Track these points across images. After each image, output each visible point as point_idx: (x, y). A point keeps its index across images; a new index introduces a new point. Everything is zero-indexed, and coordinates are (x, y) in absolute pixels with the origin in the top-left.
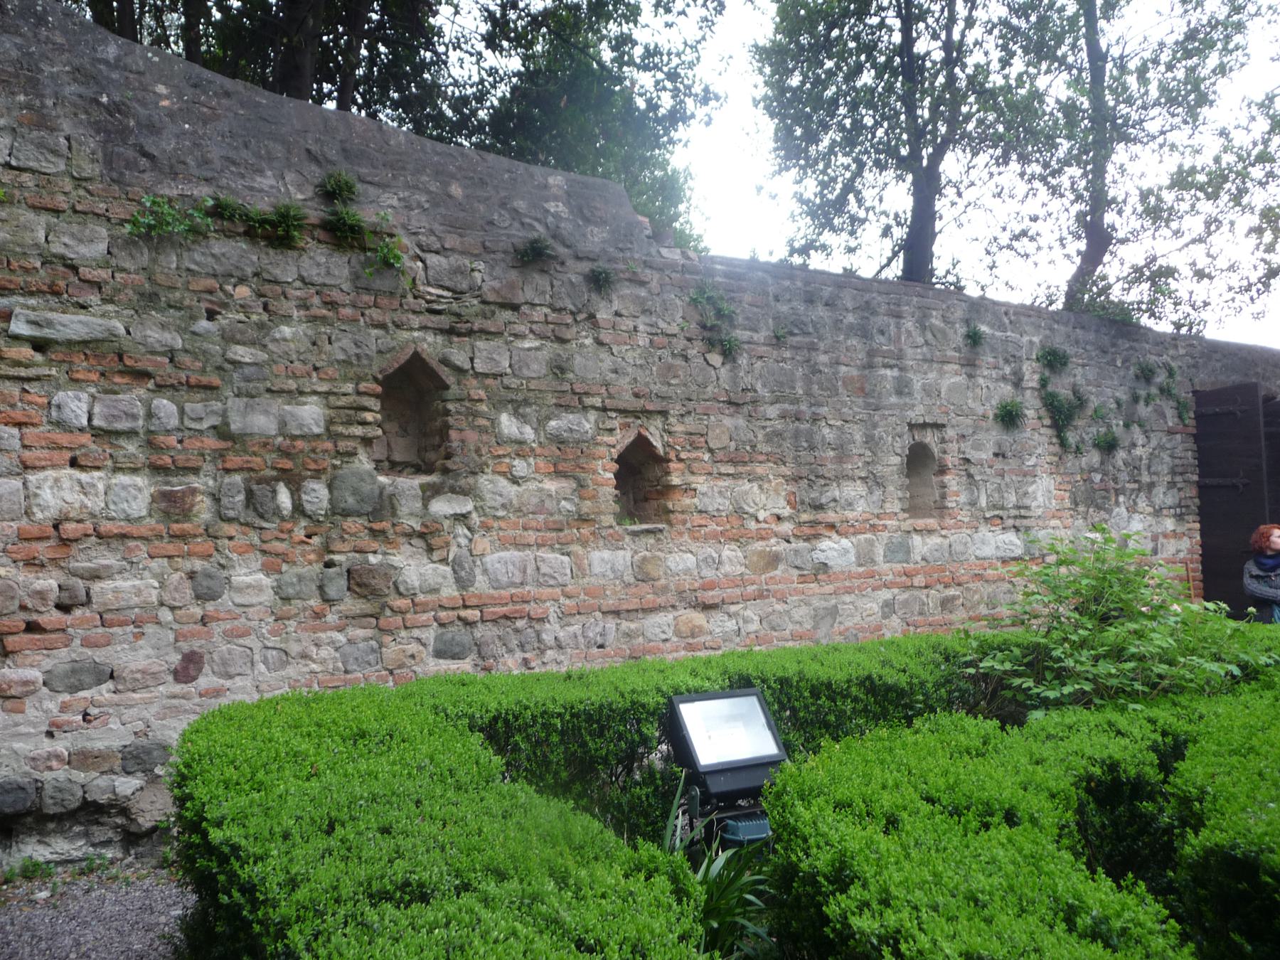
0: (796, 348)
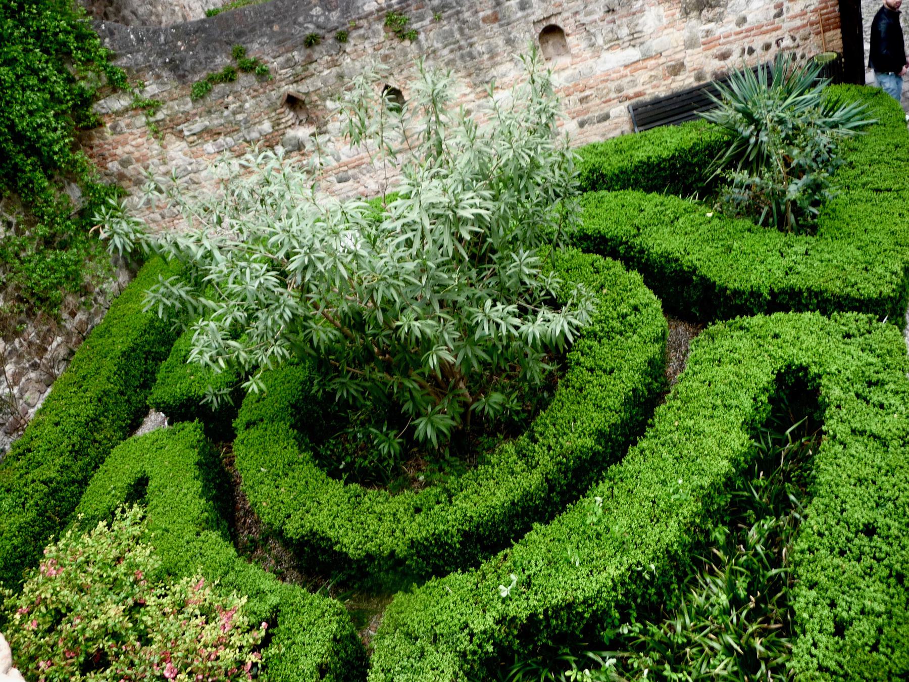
0: (449, 17)
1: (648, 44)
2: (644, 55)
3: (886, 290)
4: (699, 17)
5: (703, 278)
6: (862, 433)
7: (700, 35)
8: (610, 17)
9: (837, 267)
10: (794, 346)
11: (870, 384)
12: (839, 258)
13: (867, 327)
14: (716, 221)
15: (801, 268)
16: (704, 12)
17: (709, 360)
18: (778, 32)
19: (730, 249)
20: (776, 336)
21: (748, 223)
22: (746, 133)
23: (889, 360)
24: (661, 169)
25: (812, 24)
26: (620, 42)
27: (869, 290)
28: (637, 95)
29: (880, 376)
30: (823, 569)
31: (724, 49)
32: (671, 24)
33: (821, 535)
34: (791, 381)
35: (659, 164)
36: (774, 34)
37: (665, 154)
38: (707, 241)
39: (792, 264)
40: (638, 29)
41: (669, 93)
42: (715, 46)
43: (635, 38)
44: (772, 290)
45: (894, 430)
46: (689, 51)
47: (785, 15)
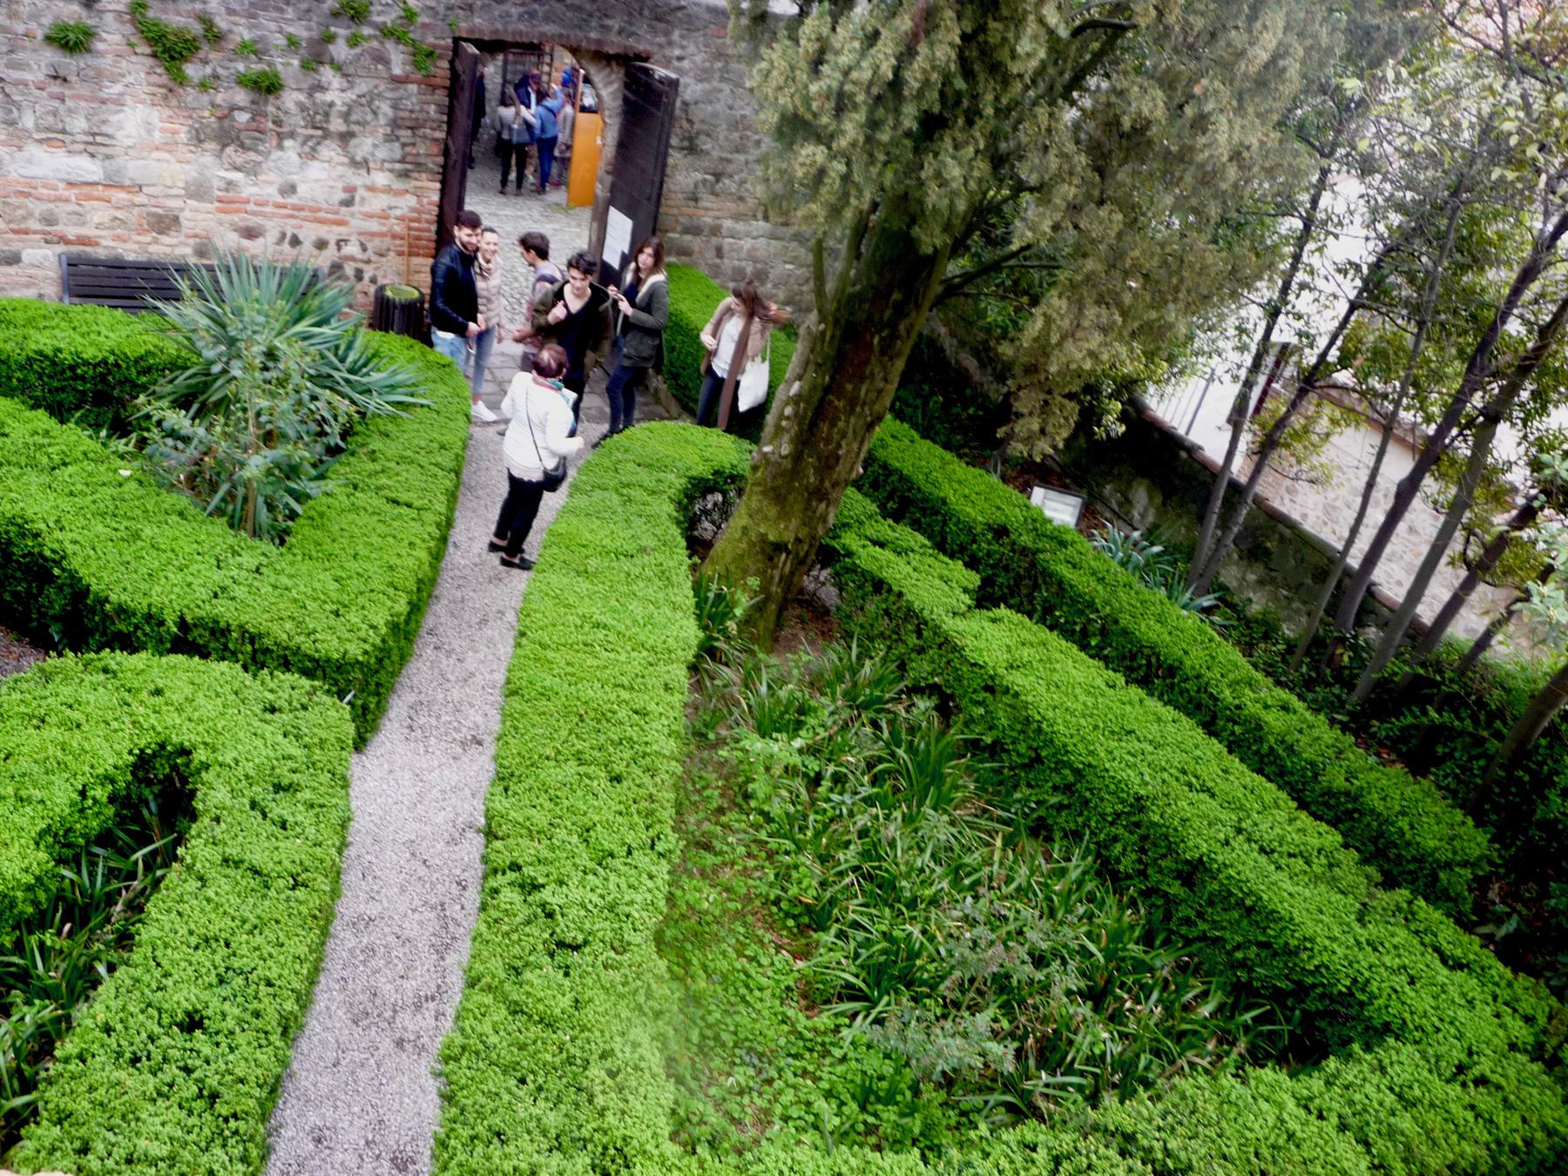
1: (120, 161)
2: (108, 177)
3: (355, 650)
4: (219, 155)
5: (74, 577)
6: (238, 864)
7: (216, 183)
8: (56, 88)
9: (295, 601)
10: (179, 710)
11: (278, 788)
12: (301, 588)
13: (305, 700)
14: (133, 485)
15: (239, 592)
16: (230, 150)
17: (23, 716)
18: (342, 229)
19: (136, 536)
20: (158, 692)
21: (183, 500)
22: (209, 354)
23: (317, 754)
24: (76, 377)
25: (394, 237)
26: (67, 138)
27: (329, 646)
28: (83, 241)
29: (295, 777)
30: (91, 1089)
31: (253, 221)
32: (169, 146)
33: (108, 1030)
34: (162, 769)
35: (72, 368)
36: (336, 229)
37: (89, 353)
38: (103, 515)
39: (228, 582)
40: (105, 129)
41: (142, 258)
42: (237, 211)
43: (96, 142)
44: (182, 618)
45: (286, 863)
46: (192, 203)
47: (356, 208)
